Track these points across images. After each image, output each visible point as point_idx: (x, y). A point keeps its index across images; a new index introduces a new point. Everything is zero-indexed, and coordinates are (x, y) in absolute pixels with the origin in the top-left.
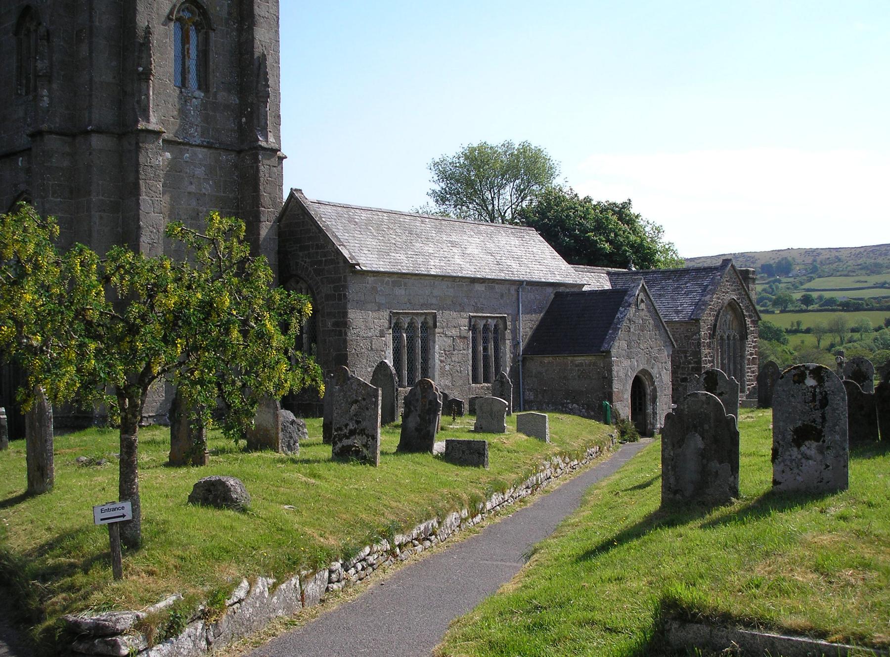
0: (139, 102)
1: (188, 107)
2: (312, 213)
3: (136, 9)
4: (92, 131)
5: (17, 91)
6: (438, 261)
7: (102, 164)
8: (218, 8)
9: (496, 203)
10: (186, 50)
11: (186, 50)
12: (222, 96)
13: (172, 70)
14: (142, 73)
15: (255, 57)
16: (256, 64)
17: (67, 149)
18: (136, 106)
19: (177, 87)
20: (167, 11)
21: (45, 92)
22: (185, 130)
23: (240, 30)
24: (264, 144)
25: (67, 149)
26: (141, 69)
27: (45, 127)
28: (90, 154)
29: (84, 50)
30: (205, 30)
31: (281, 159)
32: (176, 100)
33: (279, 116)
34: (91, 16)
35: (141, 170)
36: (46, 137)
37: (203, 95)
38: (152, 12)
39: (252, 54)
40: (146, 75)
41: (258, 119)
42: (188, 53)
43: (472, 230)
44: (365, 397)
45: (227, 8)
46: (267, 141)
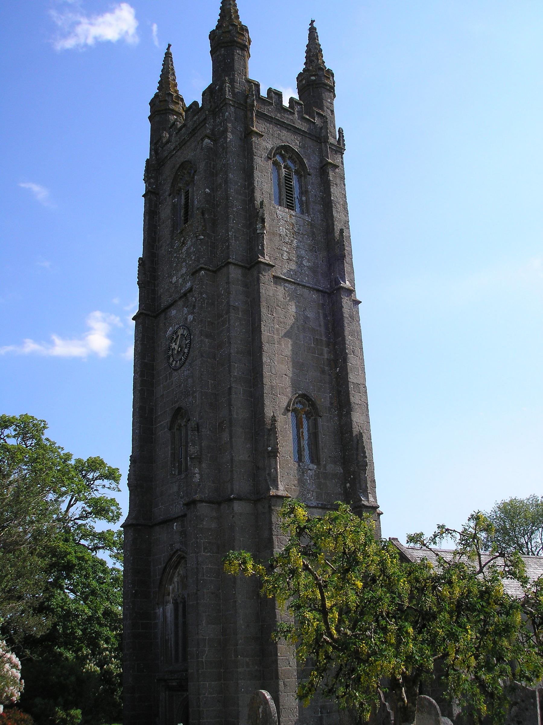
0: (269, 474)
1: (305, 477)
2: (409, 556)
3: (265, 404)
4: (234, 499)
5: (172, 472)
6: (514, 590)
7: (242, 524)
8: (322, 400)
9: (529, 546)
10: (301, 434)
11: (301, 434)
12: (330, 468)
13: (291, 449)
14: (271, 452)
15: (354, 435)
16: (355, 441)
17: (214, 514)
18: (268, 478)
19: (295, 462)
20: (286, 404)
21: (197, 470)
22: (304, 495)
23: (340, 416)
24: (366, 503)
25: (214, 514)
26: (270, 449)
27: (197, 497)
28: (233, 517)
29: (225, 436)
30: (314, 417)
31: (380, 514)
32: (296, 472)
33: (374, 481)
34: (230, 411)
35: (273, 527)
36: (199, 505)
37: (316, 467)
38: (275, 405)
39: (351, 432)
40: (274, 453)
41: (360, 482)
42: (302, 435)
43: (535, 563)
44: (524, 699)
45: (329, 399)
46: (368, 501)
